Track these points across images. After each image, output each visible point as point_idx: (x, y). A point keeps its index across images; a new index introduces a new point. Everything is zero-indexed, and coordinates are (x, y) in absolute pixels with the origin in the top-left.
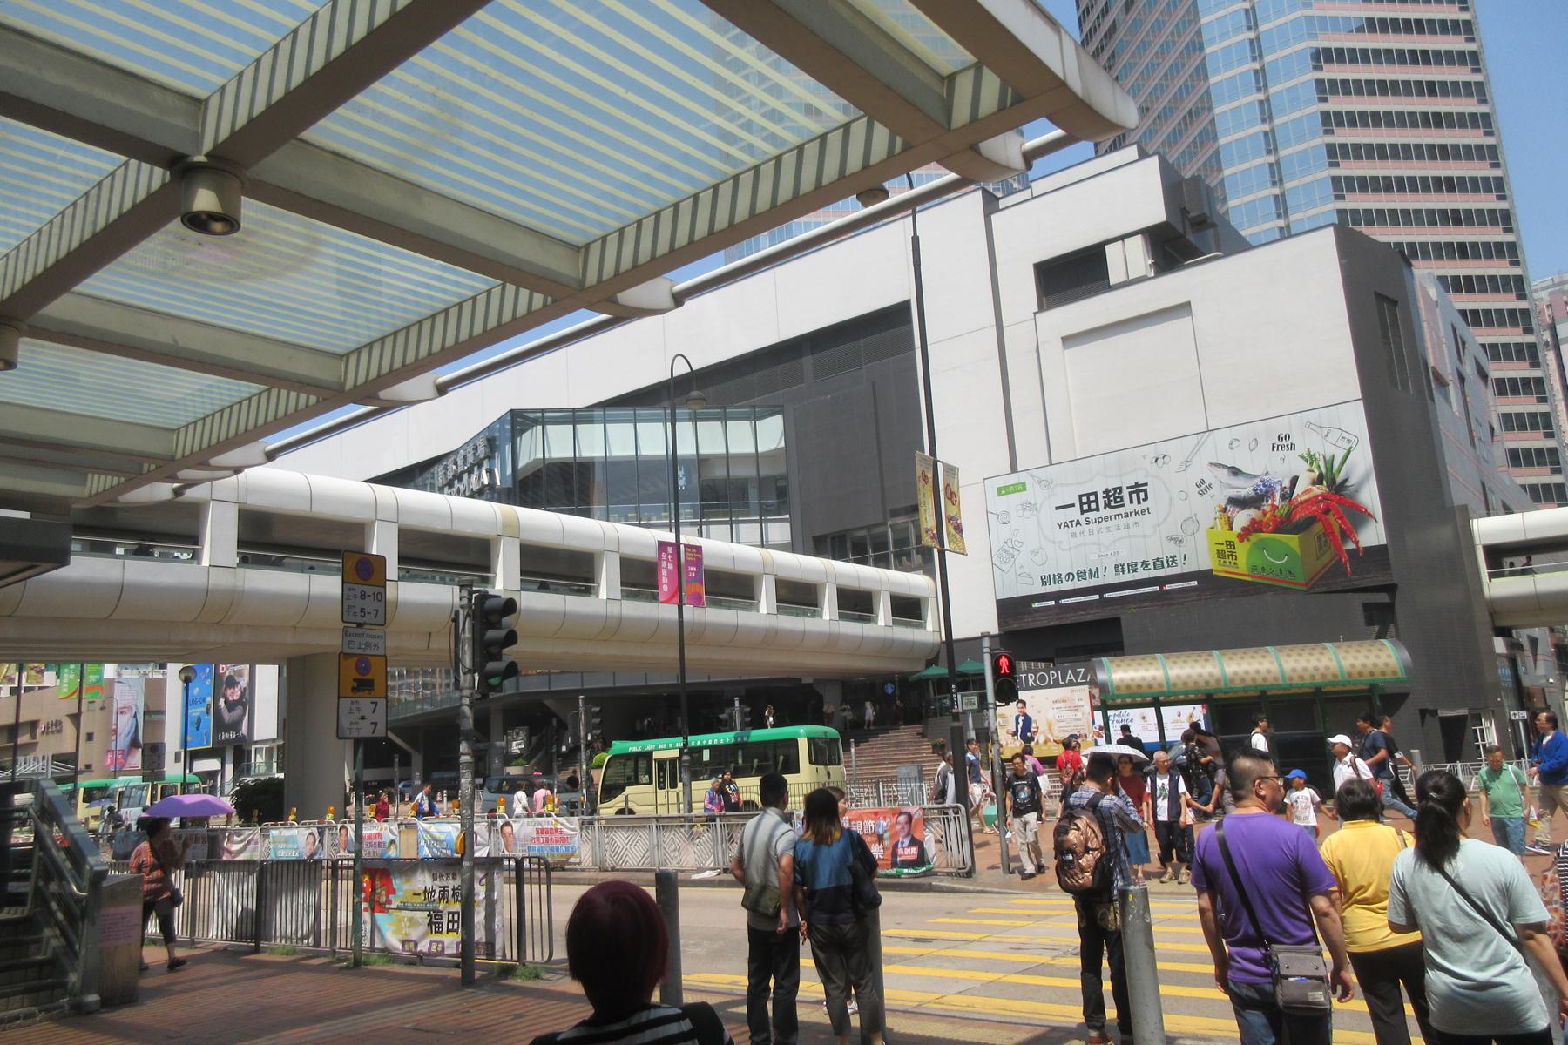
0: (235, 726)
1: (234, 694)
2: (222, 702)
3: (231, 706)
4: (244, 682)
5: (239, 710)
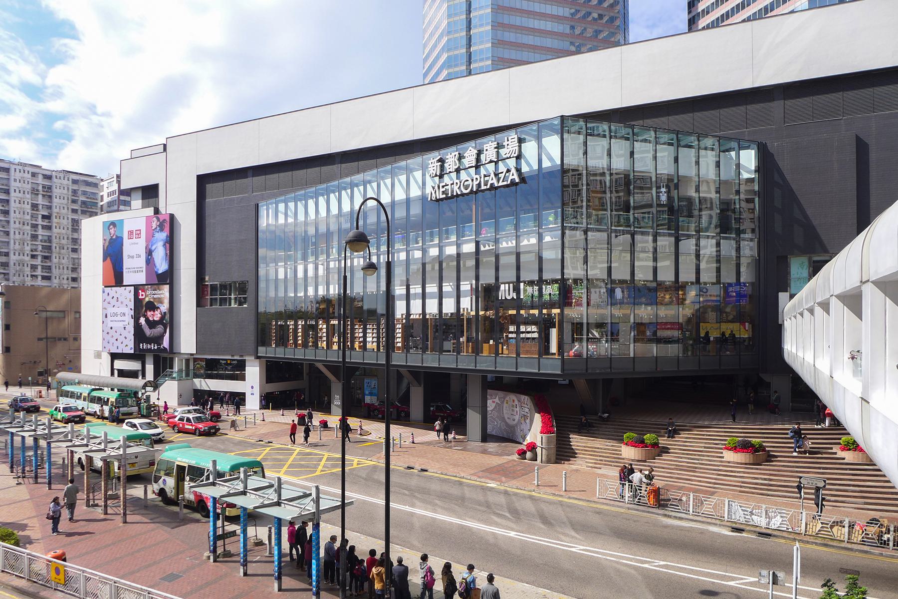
0: (158, 340)
1: (157, 316)
2: (142, 320)
3: (152, 324)
4: (165, 307)
5: (160, 329)
